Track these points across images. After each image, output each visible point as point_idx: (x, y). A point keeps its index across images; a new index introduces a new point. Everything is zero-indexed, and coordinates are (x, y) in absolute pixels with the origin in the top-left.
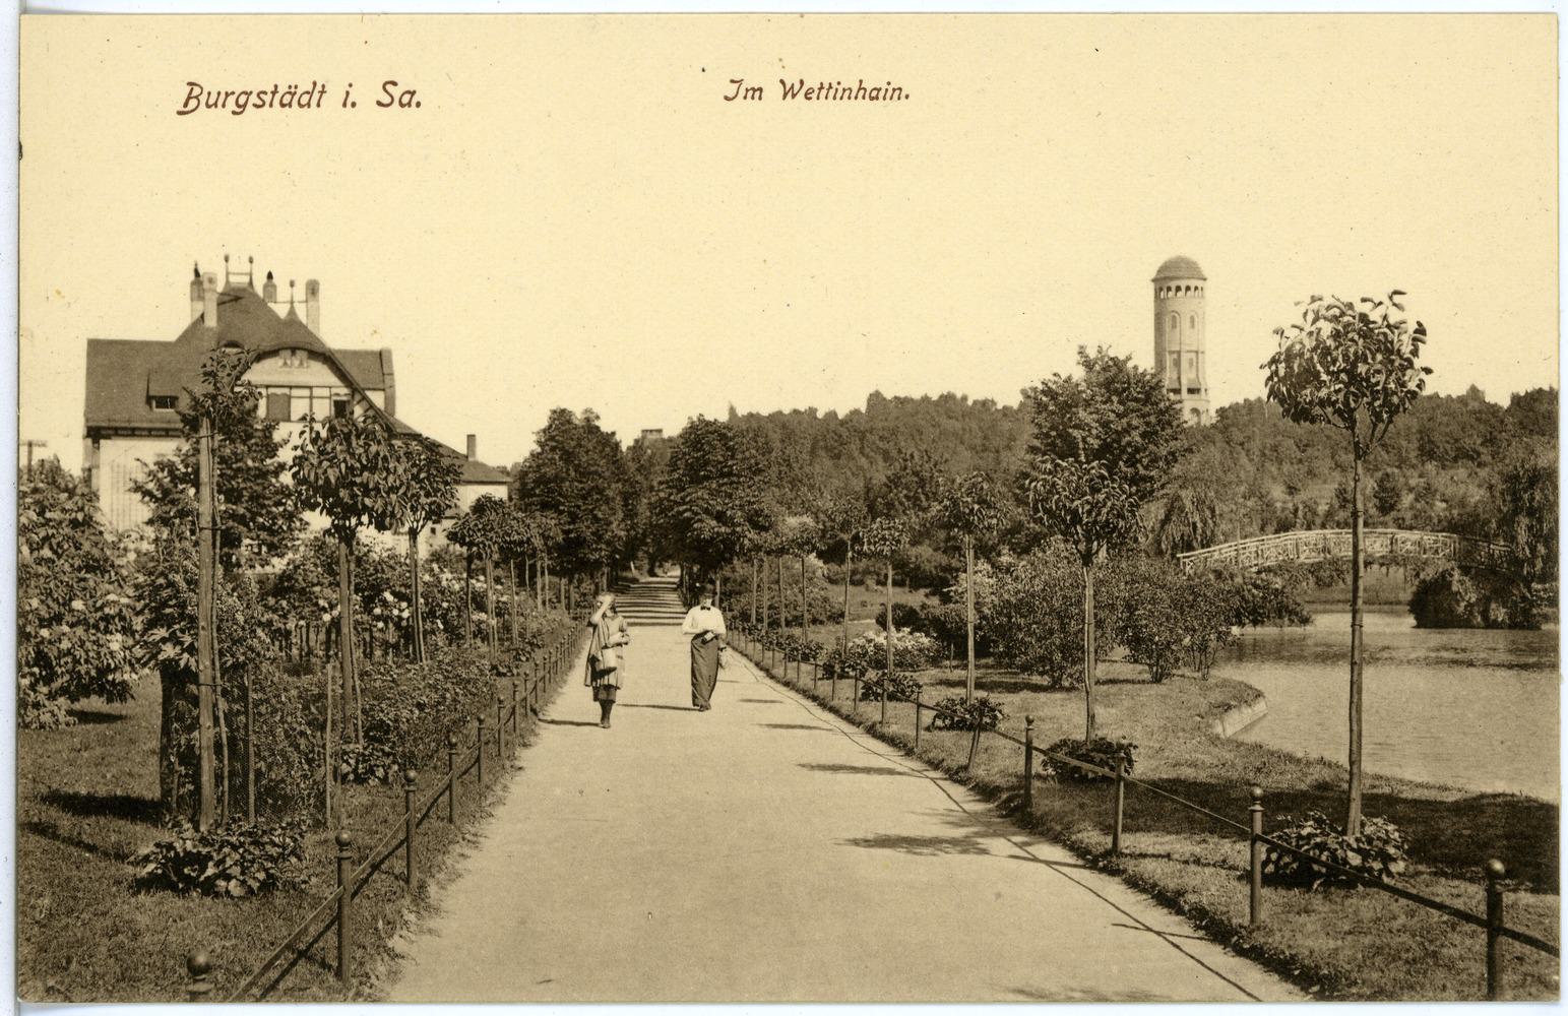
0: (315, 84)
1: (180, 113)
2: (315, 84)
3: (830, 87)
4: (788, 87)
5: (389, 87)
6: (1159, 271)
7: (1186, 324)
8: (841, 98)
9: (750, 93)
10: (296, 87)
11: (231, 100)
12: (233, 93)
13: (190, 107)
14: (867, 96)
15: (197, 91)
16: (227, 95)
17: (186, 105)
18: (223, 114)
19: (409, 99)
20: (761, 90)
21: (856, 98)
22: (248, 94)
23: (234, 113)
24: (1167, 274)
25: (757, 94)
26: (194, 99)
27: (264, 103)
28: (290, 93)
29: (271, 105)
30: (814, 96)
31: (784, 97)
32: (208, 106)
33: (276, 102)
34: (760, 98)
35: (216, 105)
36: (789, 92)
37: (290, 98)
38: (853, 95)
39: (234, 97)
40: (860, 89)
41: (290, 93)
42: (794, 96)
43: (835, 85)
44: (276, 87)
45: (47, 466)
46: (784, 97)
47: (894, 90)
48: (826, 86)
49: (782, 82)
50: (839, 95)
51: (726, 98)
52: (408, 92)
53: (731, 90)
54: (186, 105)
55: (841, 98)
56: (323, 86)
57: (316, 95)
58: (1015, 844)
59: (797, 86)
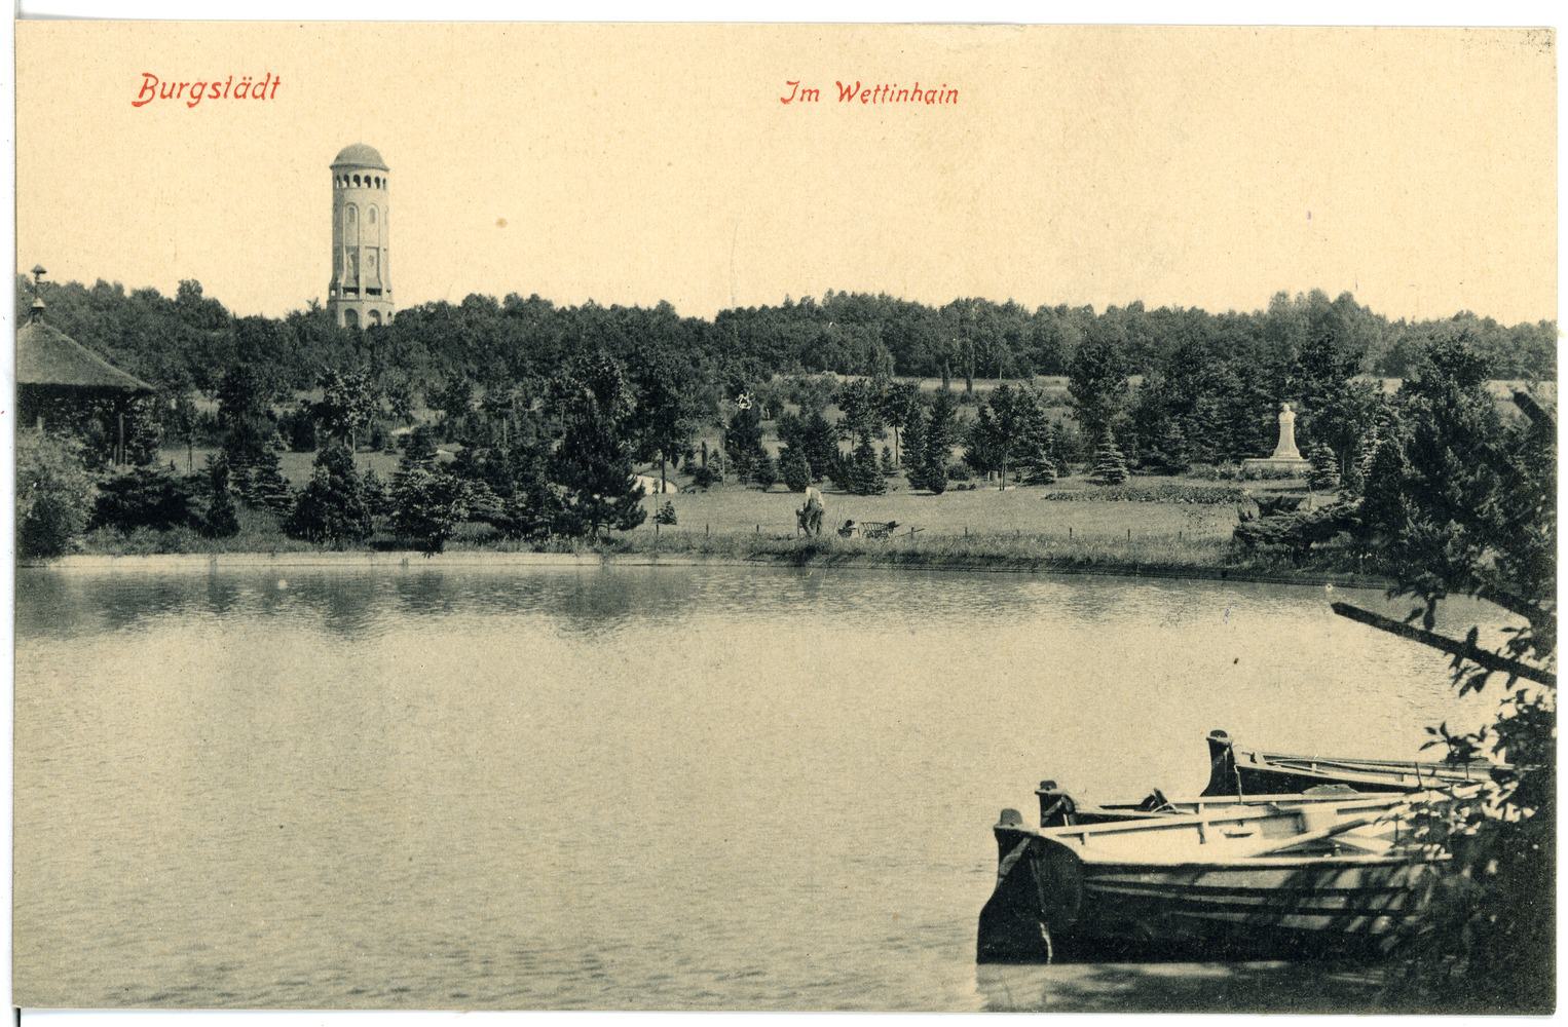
0: (269, 75)
1: (137, 104)
2: (269, 75)
3: (887, 89)
4: (845, 88)
6: (338, 158)
7: (365, 218)
10: (250, 79)
11: (186, 92)
12: (187, 84)
13: (144, 98)
16: (182, 86)
17: (141, 96)
18: (179, 104)
20: (817, 91)
21: (912, 99)
22: (204, 86)
24: (345, 162)
25: (814, 95)
26: (150, 89)
28: (244, 84)
29: (225, 95)
30: (871, 98)
32: (163, 96)
33: (231, 94)
34: (816, 100)
35: (170, 95)
36: (846, 94)
37: (244, 90)
38: (909, 97)
40: (916, 91)
42: (850, 97)
43: (891, 88)
48: (883, 88)
49: (839, 84)
50: (896, 95)
53: (787, 92)
54: (141, 96)
55: (898, 100)
56: (278, 78)
57: (270, 87)
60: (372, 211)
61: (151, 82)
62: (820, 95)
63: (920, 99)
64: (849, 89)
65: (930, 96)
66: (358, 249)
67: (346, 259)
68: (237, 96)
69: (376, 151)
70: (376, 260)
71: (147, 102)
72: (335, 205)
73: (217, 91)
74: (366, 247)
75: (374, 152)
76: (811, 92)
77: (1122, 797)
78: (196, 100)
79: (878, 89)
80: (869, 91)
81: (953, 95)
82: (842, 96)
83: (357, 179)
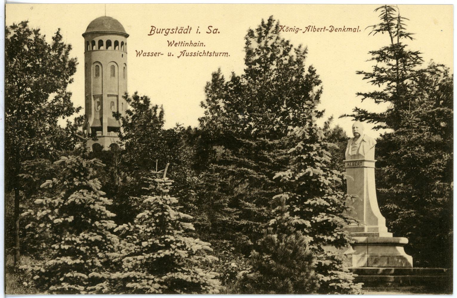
0: (188, 27)
1: (149, 35)
2: (188, 27)
4: (138, 52)
5: (210, 28)
11: (164, 31)
13: (152, 33)
15: (154, 29)
16: (163, 30)
17: (151, 33)
19: (216, 31)
22: (169, 30)
23: (165, 35)
30: (157, 55)
35: (159, 32)
39: (165, 31)
52: (216, 29)
54: (151, 33)
57: (189, 30)
59: (141, 52)
60: (113, 68)
66: (102, 97)
67: (93, 103)
68: (179, 33)
69: (111, 18)
70: (116, 104)
72: (86, 64)
74: (108, 96)
75: (116, 23)
83: (101, 43)
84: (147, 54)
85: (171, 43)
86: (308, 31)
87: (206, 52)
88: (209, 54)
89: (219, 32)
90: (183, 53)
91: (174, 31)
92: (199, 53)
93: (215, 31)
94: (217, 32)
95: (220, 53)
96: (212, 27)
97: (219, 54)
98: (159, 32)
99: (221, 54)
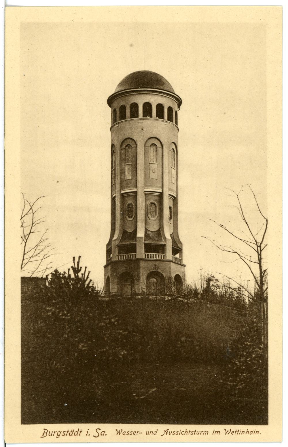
0: (79, 429)
1: (41, 437)
2: (79, 429)
3: (239, 431)
4: (118, 431)
8: (150, 434)
9: (216, 432)
10: (74, 430)
11: (56, 433)
12: (56, 432)
13: (44, 436)
14: (249, 433)
15: (46, 431)
16: (55, 432)
17: (43, 435)
22: (125, 432)
23: (57, 437)
25: (207, 433)
27: (65, 435)
28: (72, 432)
29: (67, 435)
30: (136, 433)
31: (117, 434)
32: (49, 435)
33: (181, 434)
35: (51, 435)
38: (245, 433)
40: (247, 432)
41: (72, 432)
42: (228, 434)
43: (240, 431)
44: (68, 430)
45: (207, 280)
46: (117, 434)
47: (242, 432)
48: (237, 431)
49: (117, 430)
50: (241, 433)
51: (161, 435)
52: (103, 431)
54: (43, 435)
55: (150, 434)
56: (81, 430)
57: (79, 433)
58: (179, 107)
59: (229, 431)
61: (46, 431)
62: (209, 433)
63: (248, 434)
64: (228, 431)
65: (251, 433)
71: (45, 437)
73: (64, 433)
76: (206, 432)
77: (170, 243)
78: (58, 436)
79: (236, 431)
80: (234, 432)
81: (147, 433)
82: (226, 433)
84: (126, 433)
85: (119, 431)
86: (166, 434)
87: (188, 431)
88: (191, 433)
89: (106, 435)
90: (166, 432)
91: (66, 433)
92: (181, 432)
93: (103, 433)
94: (105, 434)
95: (201, 432)
96: (100, 429)
97: (200, 432)
98: (51, 435)
99: (202, 433)
